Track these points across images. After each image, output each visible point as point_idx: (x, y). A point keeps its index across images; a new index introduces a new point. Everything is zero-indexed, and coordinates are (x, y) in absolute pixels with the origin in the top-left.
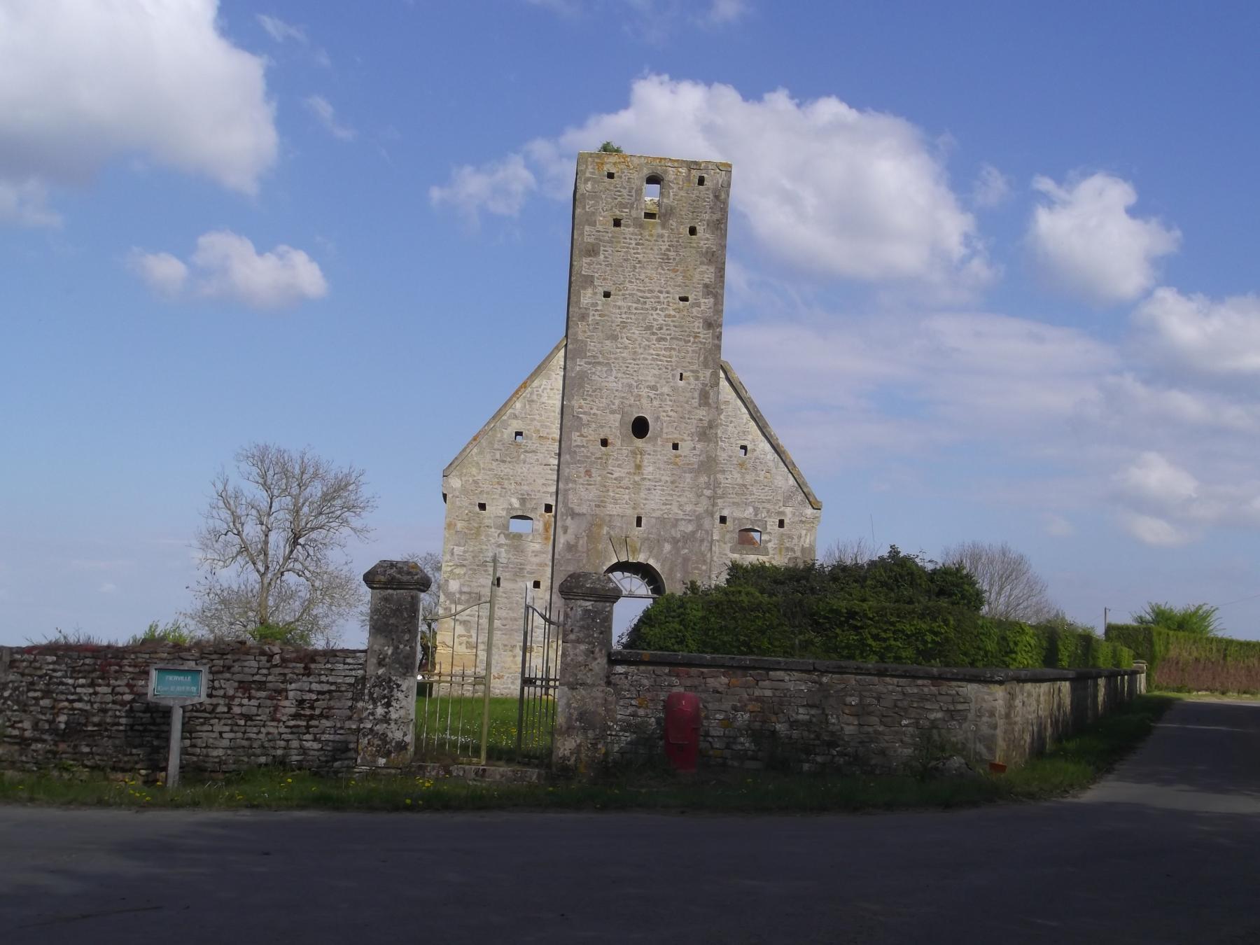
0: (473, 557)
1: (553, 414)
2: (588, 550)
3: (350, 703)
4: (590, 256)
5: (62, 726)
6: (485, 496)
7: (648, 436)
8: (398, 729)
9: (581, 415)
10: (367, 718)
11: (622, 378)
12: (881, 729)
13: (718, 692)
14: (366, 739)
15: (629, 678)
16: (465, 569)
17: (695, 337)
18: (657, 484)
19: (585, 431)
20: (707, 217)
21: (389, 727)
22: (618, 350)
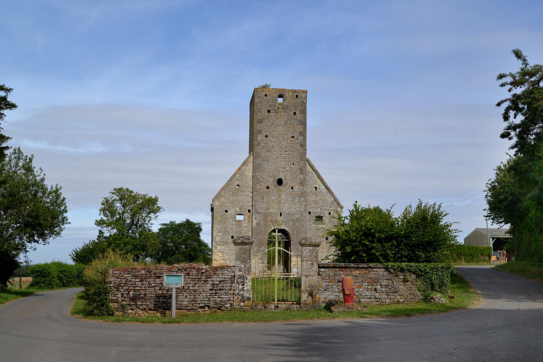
0: (224, 229)
1: (249, 178)
2: (264, 225)
5: (132, 296)
6: (227, 207)
7: (283, 185)
9: (259, 178)
11: (273, 165)
12: (412, 286)
13: (356, 276)
15: (326, 272)
16: (221, 233)
18: (286, 201)
19: (261, 184)
20: (299, 109)
21: (244, 292)
22: (271, 155)
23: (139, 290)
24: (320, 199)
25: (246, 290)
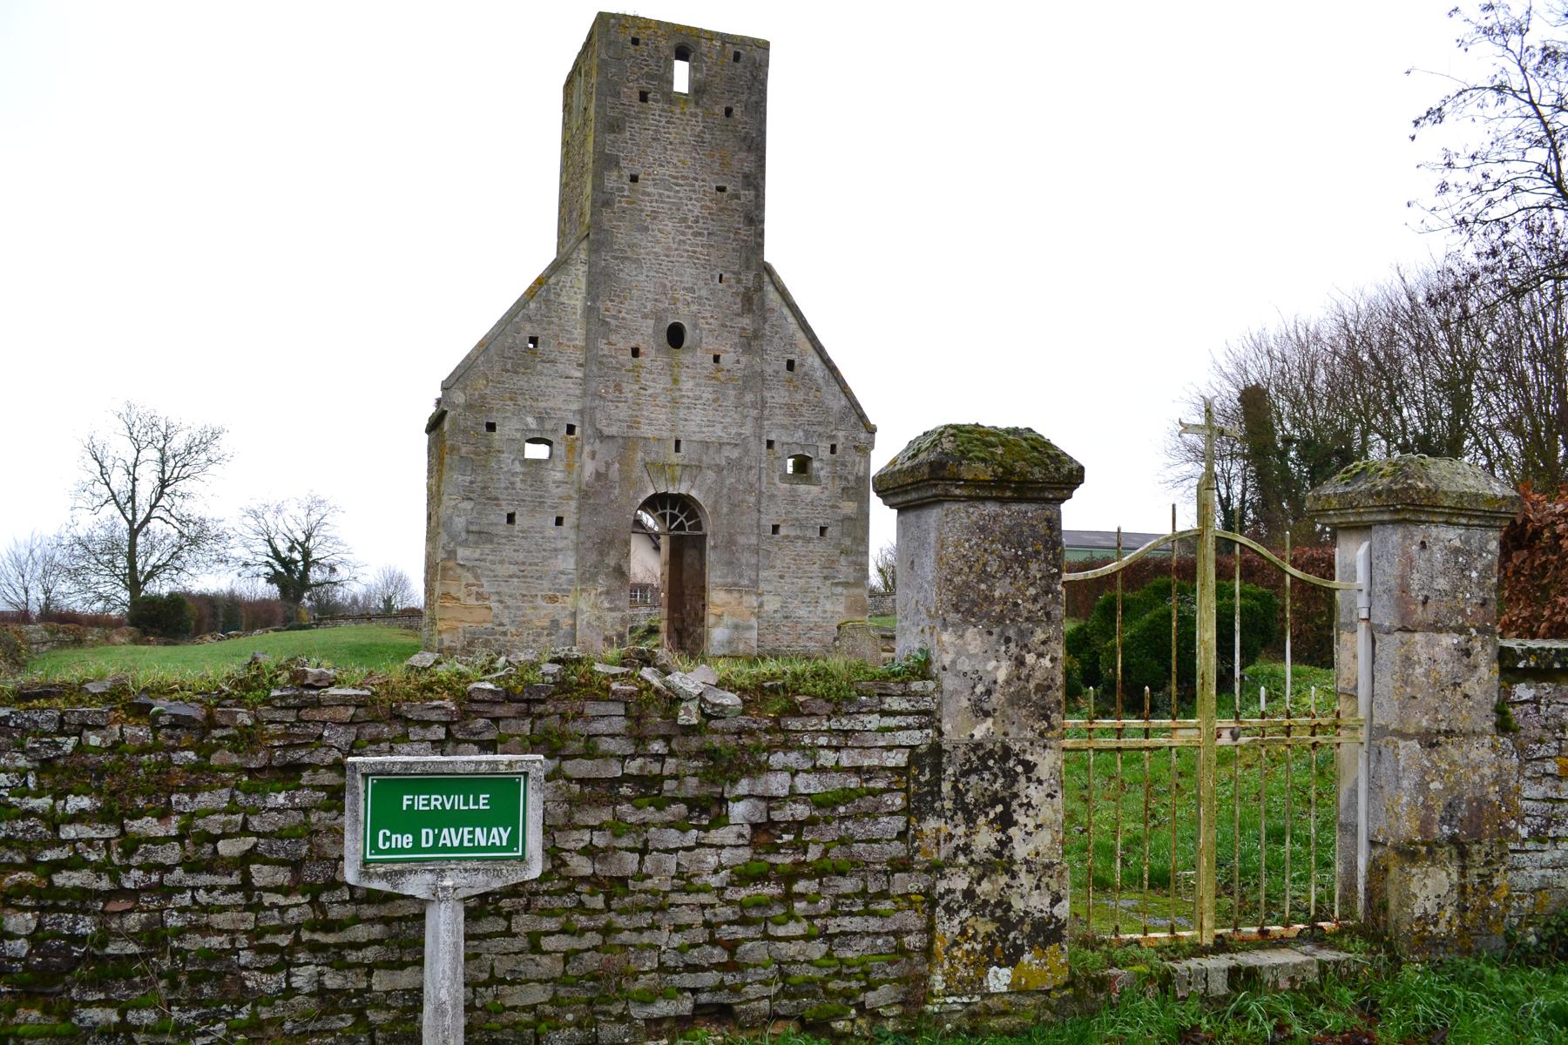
3: (899, 823)
4: (614, 132)
8: (1038, 887)
10: (950, 862)
14: (956, 922)
15: (1543, 708)
16: (472, 503)
17: (736, 233)
19: (613, 338)
20: (744, 97)
21: (1015, 883)
23: (98, 894)
24: (805, 400)
25: (1027, 862)
